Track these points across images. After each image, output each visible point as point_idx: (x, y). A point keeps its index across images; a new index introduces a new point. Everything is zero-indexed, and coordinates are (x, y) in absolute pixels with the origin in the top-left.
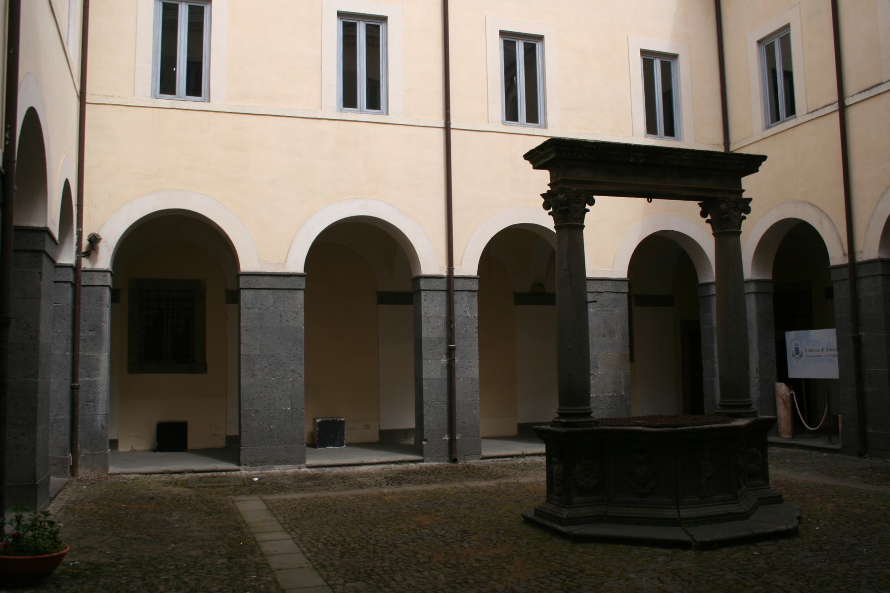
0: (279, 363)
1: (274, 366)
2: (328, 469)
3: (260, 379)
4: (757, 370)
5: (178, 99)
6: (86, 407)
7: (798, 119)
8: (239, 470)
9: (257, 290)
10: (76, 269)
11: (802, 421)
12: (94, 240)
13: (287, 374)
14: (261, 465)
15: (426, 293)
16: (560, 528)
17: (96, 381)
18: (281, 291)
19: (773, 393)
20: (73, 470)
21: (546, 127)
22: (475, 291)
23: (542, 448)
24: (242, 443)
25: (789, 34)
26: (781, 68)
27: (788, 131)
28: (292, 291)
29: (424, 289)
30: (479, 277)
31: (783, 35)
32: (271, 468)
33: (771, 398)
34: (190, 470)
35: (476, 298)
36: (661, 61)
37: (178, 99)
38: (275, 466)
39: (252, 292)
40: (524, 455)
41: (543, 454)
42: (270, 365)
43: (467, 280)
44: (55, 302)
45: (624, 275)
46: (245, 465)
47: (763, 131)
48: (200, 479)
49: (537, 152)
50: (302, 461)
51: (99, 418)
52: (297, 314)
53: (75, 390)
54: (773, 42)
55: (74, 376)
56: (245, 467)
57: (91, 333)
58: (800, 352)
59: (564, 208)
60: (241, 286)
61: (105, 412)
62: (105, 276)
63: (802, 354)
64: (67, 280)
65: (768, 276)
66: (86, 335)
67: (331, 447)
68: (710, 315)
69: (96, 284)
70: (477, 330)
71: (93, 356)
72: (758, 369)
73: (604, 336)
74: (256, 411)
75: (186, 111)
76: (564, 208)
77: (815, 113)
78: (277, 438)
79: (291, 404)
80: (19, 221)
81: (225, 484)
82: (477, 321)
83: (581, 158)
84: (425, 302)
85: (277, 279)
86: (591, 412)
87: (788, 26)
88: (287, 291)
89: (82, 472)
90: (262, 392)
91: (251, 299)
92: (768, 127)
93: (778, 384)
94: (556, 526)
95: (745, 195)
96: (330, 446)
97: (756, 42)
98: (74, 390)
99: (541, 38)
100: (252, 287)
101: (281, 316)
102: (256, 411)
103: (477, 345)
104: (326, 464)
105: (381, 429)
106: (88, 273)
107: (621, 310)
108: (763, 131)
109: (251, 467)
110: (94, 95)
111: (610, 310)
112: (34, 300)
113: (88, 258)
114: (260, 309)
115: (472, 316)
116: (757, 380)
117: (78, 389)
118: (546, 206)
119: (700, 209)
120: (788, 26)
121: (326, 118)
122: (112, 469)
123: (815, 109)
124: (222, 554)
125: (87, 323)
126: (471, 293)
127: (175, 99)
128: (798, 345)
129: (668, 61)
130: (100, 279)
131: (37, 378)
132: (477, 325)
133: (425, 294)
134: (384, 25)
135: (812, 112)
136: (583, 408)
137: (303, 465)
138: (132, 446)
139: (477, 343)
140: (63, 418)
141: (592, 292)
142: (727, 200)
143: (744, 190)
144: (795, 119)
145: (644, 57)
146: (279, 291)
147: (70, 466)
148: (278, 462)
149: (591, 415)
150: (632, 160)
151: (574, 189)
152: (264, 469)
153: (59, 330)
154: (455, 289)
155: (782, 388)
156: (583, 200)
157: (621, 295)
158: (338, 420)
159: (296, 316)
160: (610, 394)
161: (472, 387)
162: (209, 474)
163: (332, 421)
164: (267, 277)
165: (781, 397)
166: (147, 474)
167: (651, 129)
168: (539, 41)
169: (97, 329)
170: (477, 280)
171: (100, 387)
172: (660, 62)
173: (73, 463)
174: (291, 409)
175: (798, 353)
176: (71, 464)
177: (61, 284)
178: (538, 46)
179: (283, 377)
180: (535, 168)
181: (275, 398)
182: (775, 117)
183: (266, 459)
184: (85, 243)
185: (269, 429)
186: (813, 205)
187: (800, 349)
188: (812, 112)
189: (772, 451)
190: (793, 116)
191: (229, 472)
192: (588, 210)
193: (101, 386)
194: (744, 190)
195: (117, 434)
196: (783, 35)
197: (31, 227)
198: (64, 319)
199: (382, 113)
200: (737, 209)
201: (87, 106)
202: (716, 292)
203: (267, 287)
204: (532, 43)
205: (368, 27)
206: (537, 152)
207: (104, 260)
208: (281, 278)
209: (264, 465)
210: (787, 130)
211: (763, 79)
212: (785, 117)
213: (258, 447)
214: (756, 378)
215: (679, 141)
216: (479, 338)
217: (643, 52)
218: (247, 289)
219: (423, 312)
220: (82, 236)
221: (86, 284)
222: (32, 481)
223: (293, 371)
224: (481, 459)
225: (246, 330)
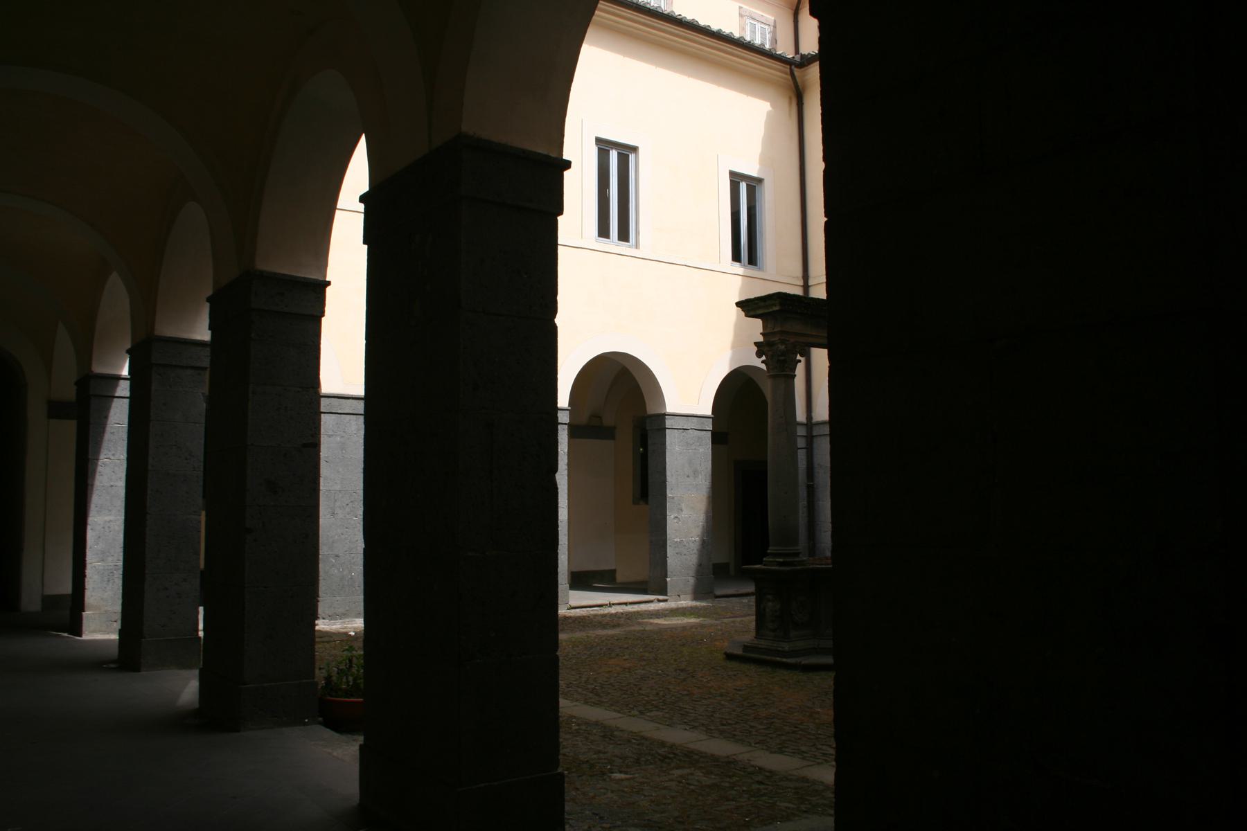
1: (357, 504)
3: (342, 518)
14: (341, 619)
16: (784, 660)
21: (637, 246)
22: (565, 424)
23: (751, 588)
24: (320, 593)
30: (570, 408)
32: (352, 621)
40: (611, 605)
41: (751, 594)
42: (352, 502)
44: (117, 422)
45: (708, 411)
46: (324, 619)
49: (756, 302)
56: (324, 620)
59: (782, 358)
70: (567, 467)
73: (688, 476)
74: (337, 556)
76: (782, 358)
90: (342, 534)
94: (778, 659)
99: (634, 149)
100: (333, 411)
102: (337, 556)
107: (704, 449)
111: (695, 449)
112: (197, 425)
129: (754, 184)
132: (567, 461)
136: (792, 548)
145: (619, 151)
151: (792, 340)
152: (344, 623)
157: (705, 432)
164: (351, 400)
170: (568, 412)
178: (632, 157)
180: (746, 316)
181: (357, 541)
183: (347, 611)
185: (350, 577)
202: (130, 373)
203: (351, 412)
204: (626, 151)
206: (756, 302)
209: (344, 618)
213: (338, 598)
216: (568, 475)
218: (328, 413)
224: (568, 609)
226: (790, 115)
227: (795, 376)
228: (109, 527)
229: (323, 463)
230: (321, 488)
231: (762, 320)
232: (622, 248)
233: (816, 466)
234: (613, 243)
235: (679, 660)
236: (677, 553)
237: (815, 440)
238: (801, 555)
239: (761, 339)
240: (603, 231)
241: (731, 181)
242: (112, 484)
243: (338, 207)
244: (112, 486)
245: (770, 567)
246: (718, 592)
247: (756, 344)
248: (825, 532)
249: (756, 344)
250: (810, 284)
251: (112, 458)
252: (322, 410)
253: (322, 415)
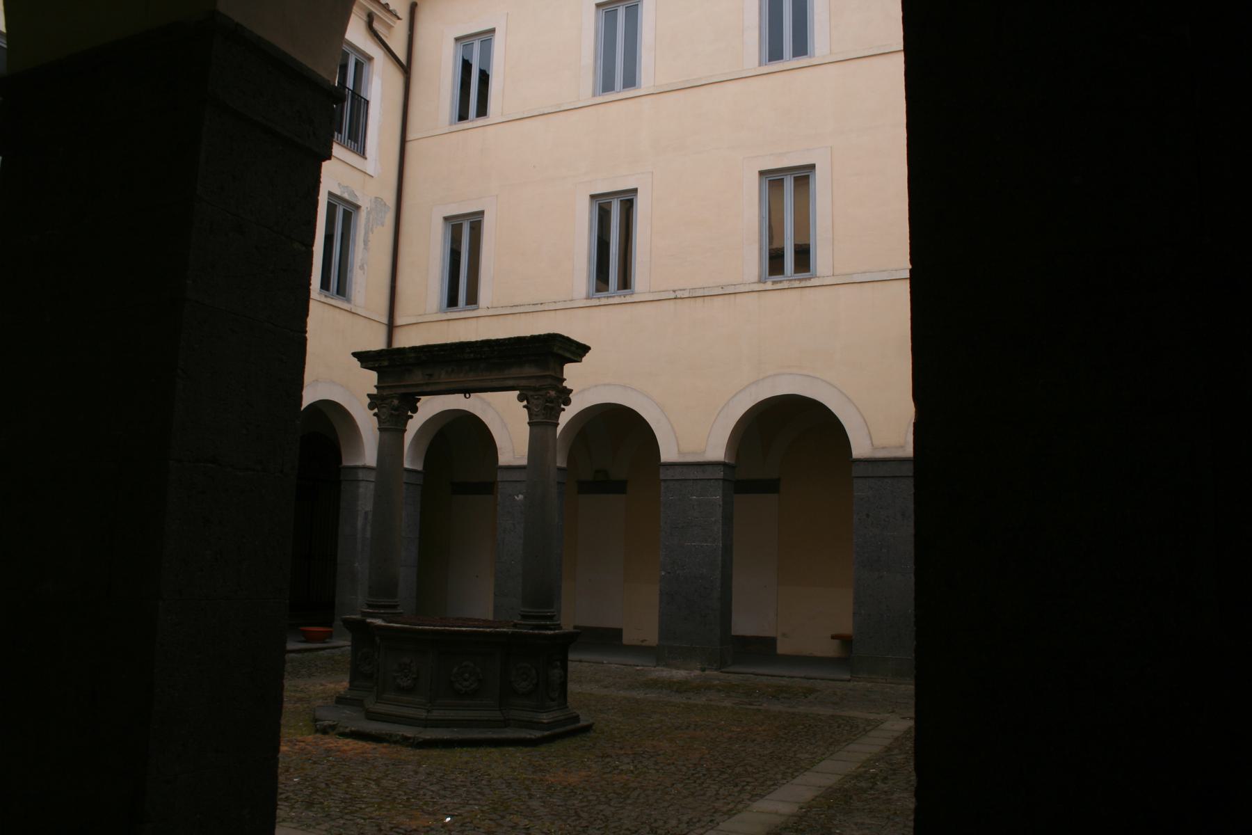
36: (344, 209)
54: (462, 224)
65: (419, 467)
87: (635, 191)
97: (588, 197)
118: (371, 407)
227: (406, 430)
231: (378, 373)
235: (701, 775)
238: (399, 608)
239: (375, 391)
241: (329, 203)
246: (723, 670)
247: (369, 396)
249: (369, 396)
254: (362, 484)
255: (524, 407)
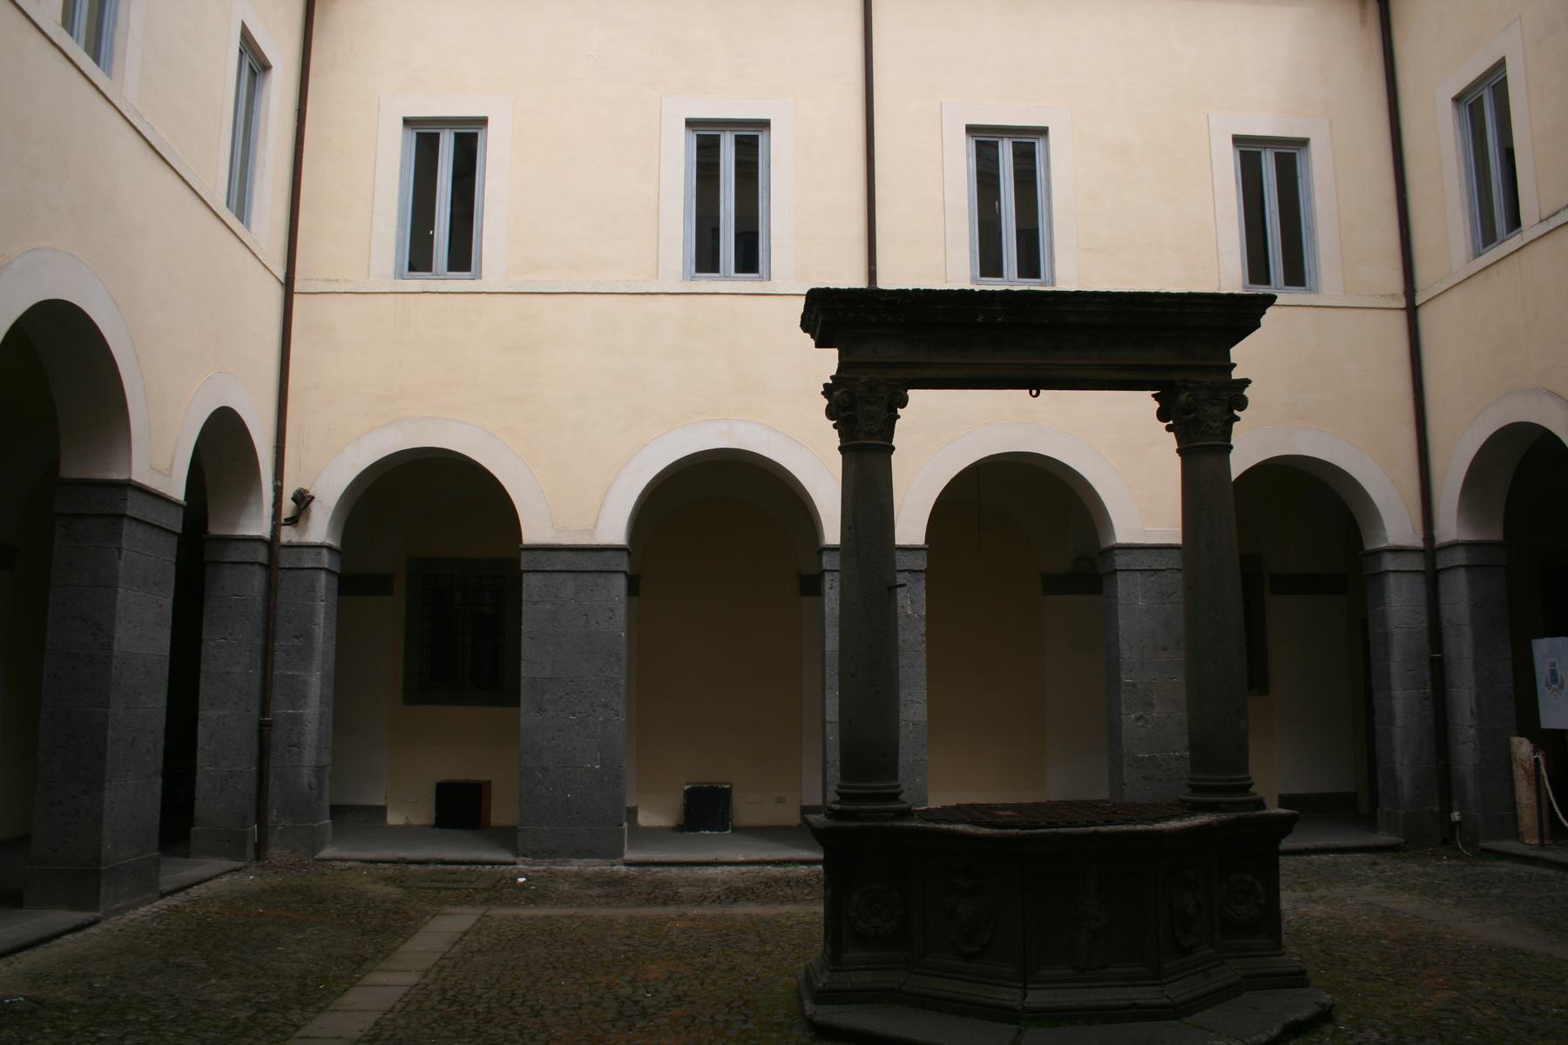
0: (581, 692)
2: (674, 870)
4: (1472, 712)
5: (436, 277)
6: (287, 754)
7: (1524, 234)
8: (514, 863)
9: (548, 574)
10: (272, 544)
11: (1556, 813)
12: (303, 500)
13: (594, 711)
14: (550, 858)
15: (832, 575)
17: (302, 715)
18: (588, 574)
19: (1507, 758)
20: (260, 851)
22: (921, 571)
25: (1506, 77)
26: (1496, 142)
27: (1510, 258)
28: (607, 574)
29: (828, 568)
31: (1495, 81)
33: (1499, 766)
34: (438, 859)
35: (923, 584)
36: (1276, 154)
37: (436, 277)
38: (573, 860)
39: (541, 576)
42: (567, 694)
43: (906, 553)
45: (1176, 538)
46: (525, 856)
47: (1468, 262)
48: (453, 873)
50: (618, 853)
51: (306, 771)
52: (613, 611)
53: (264, 728)
54: (1481, 96)
55: (264, 707)
57: (296, 640)
58: (1559, 677)
60: (523, 568)
61: (314, 763)
62: (320, 553)
63: (1563, 682)
64: (252, 561)
65: (1495, 534)
66: (290, 644)
67: (708, 832)
68: (1381, 608)
69: (306, 566)
71: (299, 676)
72: (1475, 711)
74: (544, 769)
75: (445, 295)
77: (1552, 219)
78: (577, 813)
79: (601, 759)
80: (73, 469)
81: (464, 885)
82: (925, 622)
83: (875, 321)
84: (832, 591)
85: (580, 555)
86: (1250, 785)
87: (1501, 65)
88: (597, 574)
89: (276, 853)
91: (540, 588)
92: (1477, 255)
93: (1516, 740)
95: (1236, 374)
96: (705, 831)
98: (264, 729)
100: (540, 569)
101: (586, 615)
103: (924, 665)
104: (656, 860)
105: (805, 804)
106: (296, 549)
108: (1468, 262)
109: (534, 858)
110: (311, 280)
113: (295, 527)
114: (554, 604)
115: (916, 615)
116: (1472, 731)
117: (270, 726)
119: (1156, 405)
120: (1501, 65)
121: (665, 291)
122: (328, 852)
123: (1553, 210)
124: (224, 992)
125: (291, 626)
126: (913, 574)
127: (430, 277)
128: (1554, 665)
129: (1289, 153)
130: (312, 559)
131: (109, 707)
132: (924, 629)
133: (832, 578)
134: (765, 133)
135: (1547, 219)
137: (618, 860)
138: (407, 818)
139: (925, 661)
140: (241, 769)
141: (1142, 570)
142: (1191, 385)
143: (1235, 365)
144: (1519, 235)
146: (585, 574)
147: (255, 844)
148: (578, 854)
149: (1251, 790)
150: (980, 319)
151: (864, 379)
152: (555, 864)
153: (240, 636)
154: (898, 568)
155: (1523, 748)
156: (883, 398)
158: (719, 786)
159: (611, 615)
160: (1177, 753)
161: (913, 738)
162: (463, 867)
163: (708, 787)
164: (564, 552)
165: (1522, 765)
166: (372, 862)
167: (990, 263)
168: (1041, 138)
169: (306, 635)
170: (925, 553)
171: (309, 725)
172: (1011, 144)
173: (258, 839)
174: (602, 767)
175: (1557, 680)
176: (256, 841)
177: (245, 567)
179: (589, 715)
181: (574, 749)
182: (1488, 237)
184: (288, 506)
186: (1556, 394)
187: (1560, 673)
188: (1547, 219)
189: (1285, 863)
190: (1518, 230)
191: (496, 866)
192: (1238, 419)
193: (310, 722)
194: (1235, 365)
195: (386, 798)
196: (1495, 81)
197: (107, 480)
198: (248, 619)
199: (761, 278)
200: (1215, 402)
201: (296, 297)
203: (564, 568)
205: (740, 141)
207: (319, 529)
208: (587, 554)
210: (1508, 256)
211: (1467, 166)
212: (1505, 231)
214: (1471, 727)
215: (1314, 293)
217: (1238, 140)
219: (827, 609)
220: (281, 493)
221: (291, 566)
222: (95, 864)
223: (605, 705)
225: (531, 638)
226: (1363, 22)
228: (224, 724)
229: (525, 641)
230: (523, 675)
232: (747, 283)
233: (1445, 624)
234: (728, 281)
236: (1144, 778)
237: (1443, 578)
240: (706, 260)
242: (228, 670)
243: (295, 291)
244: (228, 673)
245: (951, 827)
248: (1463, 743)
250: (1418, 302)
251: (229, 638)
252: (523, 568)
253: (525, 576)
254: (1392, 578)
255: (1169, 429)
